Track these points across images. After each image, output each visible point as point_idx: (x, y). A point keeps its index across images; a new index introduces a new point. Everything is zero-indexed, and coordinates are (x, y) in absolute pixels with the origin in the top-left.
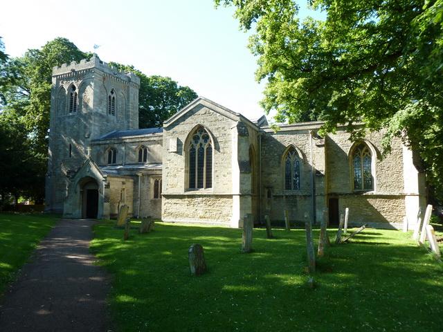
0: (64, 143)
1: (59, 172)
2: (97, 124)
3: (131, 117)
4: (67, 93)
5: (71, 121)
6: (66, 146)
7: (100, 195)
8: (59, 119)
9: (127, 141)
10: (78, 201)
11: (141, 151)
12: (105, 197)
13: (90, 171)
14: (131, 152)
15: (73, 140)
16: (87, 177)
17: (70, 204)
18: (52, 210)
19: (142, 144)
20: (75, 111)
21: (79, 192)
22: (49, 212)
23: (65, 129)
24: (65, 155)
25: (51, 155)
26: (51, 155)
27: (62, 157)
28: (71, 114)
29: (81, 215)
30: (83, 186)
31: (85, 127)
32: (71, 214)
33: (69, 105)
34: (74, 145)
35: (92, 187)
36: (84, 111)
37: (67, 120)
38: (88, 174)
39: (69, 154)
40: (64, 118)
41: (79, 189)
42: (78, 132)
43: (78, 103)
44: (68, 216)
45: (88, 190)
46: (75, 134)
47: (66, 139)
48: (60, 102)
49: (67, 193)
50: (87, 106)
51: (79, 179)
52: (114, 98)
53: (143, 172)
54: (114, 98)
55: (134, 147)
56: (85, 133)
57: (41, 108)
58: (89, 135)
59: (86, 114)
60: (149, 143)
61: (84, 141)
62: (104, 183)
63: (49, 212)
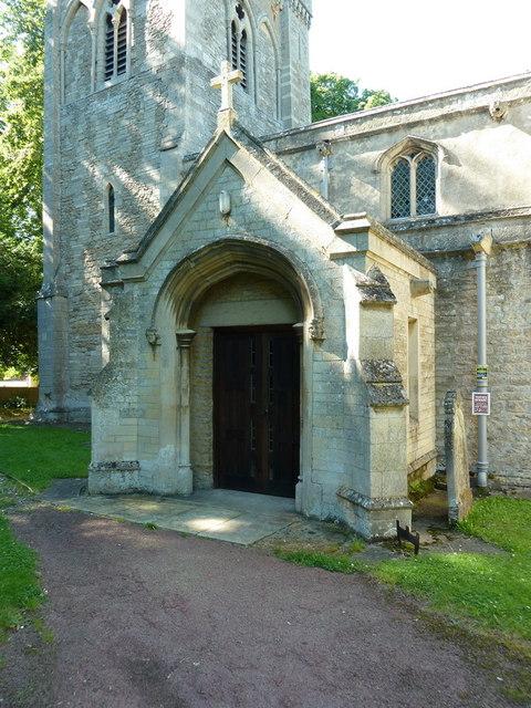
0: (89, 184)
1: (78, 284)
2: (199, 101)
3: (294, 109)
4: (92, 19)
5: (110, 106)
6: (98, 195)
7: (314, 361)
8: (72, 107)
9: (339, 133)
10: (168, 397)
11: (401, 172)
12: (372, 367)
13: (239, 207)
14: (355, 181)
15: (118, 171)
16: (229, 244)
17: (126, 414)
18: (59, 410)
19: (416, 133)
20: (121, 69)
21: (170, 343)
22: (52, 416)
23: (90, 136)
24: (95, 225)
25: (51, 228)
26: (51, 228)
27: (85, 234)
28: (108, 84)
29: (186, 473)
30: (192, 310)
31: (161, 114)
32: (132, 467)
33: (101, 57)
34: (125, 189)
35: (248, 311)
36: (154, 59)
37: (97, 105)
38: (231, 229)
39: (106, 223)
40: (88, 101)
41: (169, 325)
42: (137, 140)
43: (130, 41)
44: (118, 480)
45: (221, 333)
46: (126, 148)
47: (97, 172)
48: (74, 55)
49: (105, 351)
50: (162, 39)
51: (166, 266)
52: (244, 32)
53: (498, 229)
54: (244, 32)
55: (371, 156)
56: (161, 134)
57: (30, 126)
58: (177, 139)
59: (161, 69)
60: (450, 127)
61: (157, 166)
62: (349, 282)
63: (52, 416)
